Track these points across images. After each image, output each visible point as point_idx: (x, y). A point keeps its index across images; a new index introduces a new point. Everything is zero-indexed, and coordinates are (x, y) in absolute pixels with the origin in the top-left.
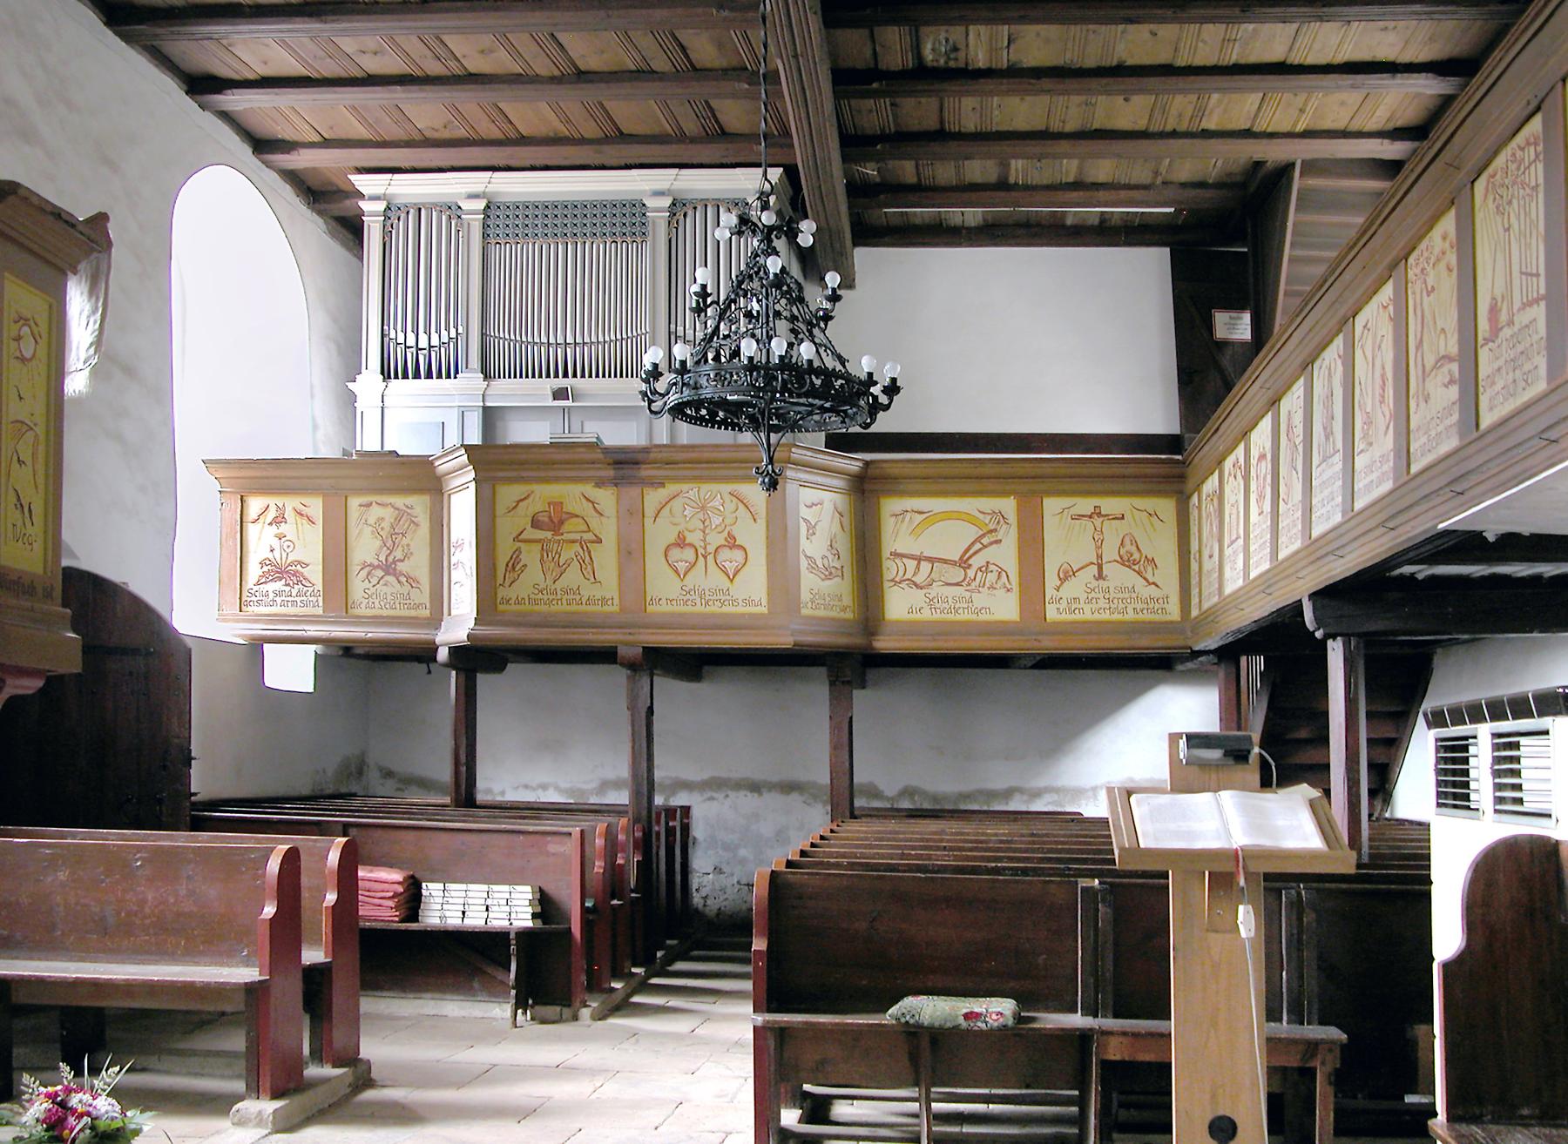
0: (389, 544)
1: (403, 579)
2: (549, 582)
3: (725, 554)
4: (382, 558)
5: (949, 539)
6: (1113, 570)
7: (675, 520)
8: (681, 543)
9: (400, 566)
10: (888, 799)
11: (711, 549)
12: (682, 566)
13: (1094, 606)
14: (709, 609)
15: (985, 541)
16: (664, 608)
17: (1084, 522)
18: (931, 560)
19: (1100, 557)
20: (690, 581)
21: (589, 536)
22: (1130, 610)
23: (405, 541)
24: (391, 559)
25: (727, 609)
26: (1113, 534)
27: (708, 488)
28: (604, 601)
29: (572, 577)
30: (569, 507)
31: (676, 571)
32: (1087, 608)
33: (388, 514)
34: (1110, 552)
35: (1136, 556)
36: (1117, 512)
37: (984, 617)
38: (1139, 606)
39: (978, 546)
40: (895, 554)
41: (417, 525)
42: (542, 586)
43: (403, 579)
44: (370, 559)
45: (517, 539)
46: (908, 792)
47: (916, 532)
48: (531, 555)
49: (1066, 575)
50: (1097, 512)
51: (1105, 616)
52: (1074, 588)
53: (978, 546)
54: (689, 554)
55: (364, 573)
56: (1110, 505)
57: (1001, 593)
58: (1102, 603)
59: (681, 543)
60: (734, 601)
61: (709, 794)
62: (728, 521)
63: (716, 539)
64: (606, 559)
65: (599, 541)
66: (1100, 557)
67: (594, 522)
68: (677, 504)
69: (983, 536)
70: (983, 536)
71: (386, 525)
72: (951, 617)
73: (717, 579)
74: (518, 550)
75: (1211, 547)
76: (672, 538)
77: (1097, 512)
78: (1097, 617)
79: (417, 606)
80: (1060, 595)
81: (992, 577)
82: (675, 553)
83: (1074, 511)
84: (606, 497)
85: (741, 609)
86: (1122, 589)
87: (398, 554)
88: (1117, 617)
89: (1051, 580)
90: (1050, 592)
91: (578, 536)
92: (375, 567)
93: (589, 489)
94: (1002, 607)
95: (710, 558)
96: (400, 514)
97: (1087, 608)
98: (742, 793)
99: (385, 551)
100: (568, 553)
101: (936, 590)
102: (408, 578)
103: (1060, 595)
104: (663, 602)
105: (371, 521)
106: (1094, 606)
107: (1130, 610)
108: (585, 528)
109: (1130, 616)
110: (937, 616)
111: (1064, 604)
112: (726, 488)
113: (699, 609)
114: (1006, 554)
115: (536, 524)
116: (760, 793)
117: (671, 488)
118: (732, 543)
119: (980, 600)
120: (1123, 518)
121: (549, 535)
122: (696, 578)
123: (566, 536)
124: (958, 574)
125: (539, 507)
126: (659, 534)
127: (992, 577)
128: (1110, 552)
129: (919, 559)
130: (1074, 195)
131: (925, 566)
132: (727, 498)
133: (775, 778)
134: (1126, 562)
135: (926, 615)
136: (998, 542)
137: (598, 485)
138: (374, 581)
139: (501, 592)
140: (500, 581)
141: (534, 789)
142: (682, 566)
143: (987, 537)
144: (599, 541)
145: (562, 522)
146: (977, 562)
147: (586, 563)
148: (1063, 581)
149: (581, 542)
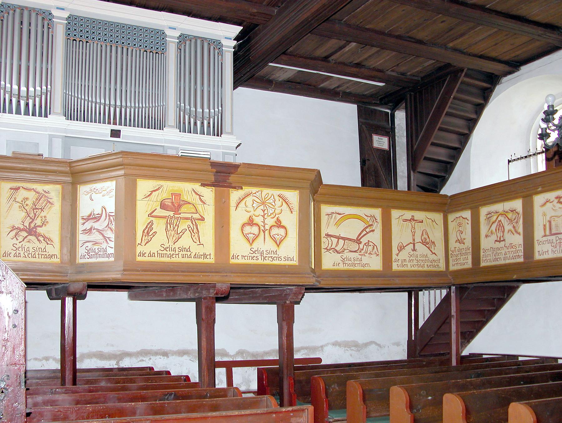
0: (32, 215)
1: (42, 239)
2: (171, 243)
3: (275, 231)
4: (27, 224)
5: (352, 229)
6: (419, 246)
7: (248, 209)
8: (251, 222)
9: (39, 230)
10: (231, 356)
11: (267, 227)
12: (251, 236)
13: (412, 263)
14: (267, 262)
15: (368, 230)
16: (241, 261)
17: (408, 223)
18: (344, 239)
19: (414, 240)
20: (255, 246)
21: (196, 216)
22: (426, 266)
23: (43, 214)
24: (32, 225)
25: (276, 262)
26: (419, 229)
27: (266, 191)
28: (205, 256)
29: (186, 241)
30: (185, 197)
31: (248, 240)
32: (409, 264)
33: (32, 196)
34: (418, 239)
35: (428, 240)
36: (421, 219)
37: (367, 268)
38: (429, 264)
39: (365, 233)
40: (328, 235)
41: (52, 204)
42: (167, 245)
43: (42, 239)
44: (19, 225)
45: (150, 215)
46: (240, 352)
47: (338, 224)
48: (159, 226)
49: (401, 248)
50: (413, 219)
51: (416, 269)
52: (404, 255)
53: (365, 233)
54: (255, 230)
55: (13, 233)
56: (419, 215)
57: (374, 256)
58: (415, 262)
59: (251, 222)
60: (279, 258)
61: (141, 358)
62: (277, 212)
63: (270, 222)
64: (208, 230)
65: (203, 219)
66: (414, 240)
67: (200, 208)
68: (249, 200)
69: (367, 227)
70: (367, 227)
71: (29, 202)
72: (352, 268)
73: (270, 245)
74: (151, 223)
75: (65, 251)
76: (245, 220)
77: (413, 219)
78: (413, 269)
79: (51, 256)
80: (398, 258)
81: (370, 248)
82: (247, 229)
83: (404, 217)
84: (209, 193)
85: (283, 263)
86: (422, 256)
87: (38, 222)
88: (420, 269)
89: (395, 250)
90: (394, 257)
91: (189, 216)
92: (21, 230)
93: (197, 186)
94: (374, 263)
95: (267, 232)
96: (40, 196)
97: (409, 264)
98: (158, 357)
99: (28, 220)
100: (184, 225)
101: (346, 254)
102: (45, 237)
103: (398, 258)
104: (240, 257)
105: (19, 199)
106: (412, 263)
107: (426, 266)
108: (194, 211)
109: (426, 269)
110: (346, 268)
111: (400, 263)
112: (276, 192)
113: (260, 262)
114: (376, 237)
115: (163, 206)
116: (168, 357)
117: (247, 189)
118: (279, 224)
119: (365, 260)
120: (422, 222)
121: (171, 214)
122: (259, 244)
123: (182, 215)
124: (355, 247)
125: (165, 196)
126: (237, 217)
127: (370, 248)
128: (418, 239)
129: (339, 238)
130: (14, 161)
131: (341, 242)
132: (277, 198)
133: (175, 349)
134: (424, 243)
135: (341, 267)
136: (373, 231)
137: (203, 185)
138: (20, 239)
139: (139, 249)
140: (139, 241)
141: (40, 360)
142: (251, 236)
143: (368, 229)
144: (203, 219)
145: (180, 206)
146: (364, 240)
147: (195, 232)
148: (399, 251)
149: (191, 219)
